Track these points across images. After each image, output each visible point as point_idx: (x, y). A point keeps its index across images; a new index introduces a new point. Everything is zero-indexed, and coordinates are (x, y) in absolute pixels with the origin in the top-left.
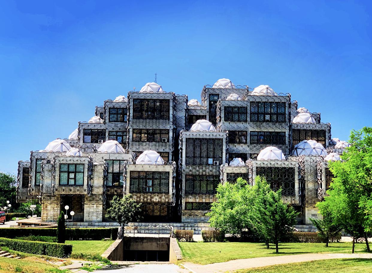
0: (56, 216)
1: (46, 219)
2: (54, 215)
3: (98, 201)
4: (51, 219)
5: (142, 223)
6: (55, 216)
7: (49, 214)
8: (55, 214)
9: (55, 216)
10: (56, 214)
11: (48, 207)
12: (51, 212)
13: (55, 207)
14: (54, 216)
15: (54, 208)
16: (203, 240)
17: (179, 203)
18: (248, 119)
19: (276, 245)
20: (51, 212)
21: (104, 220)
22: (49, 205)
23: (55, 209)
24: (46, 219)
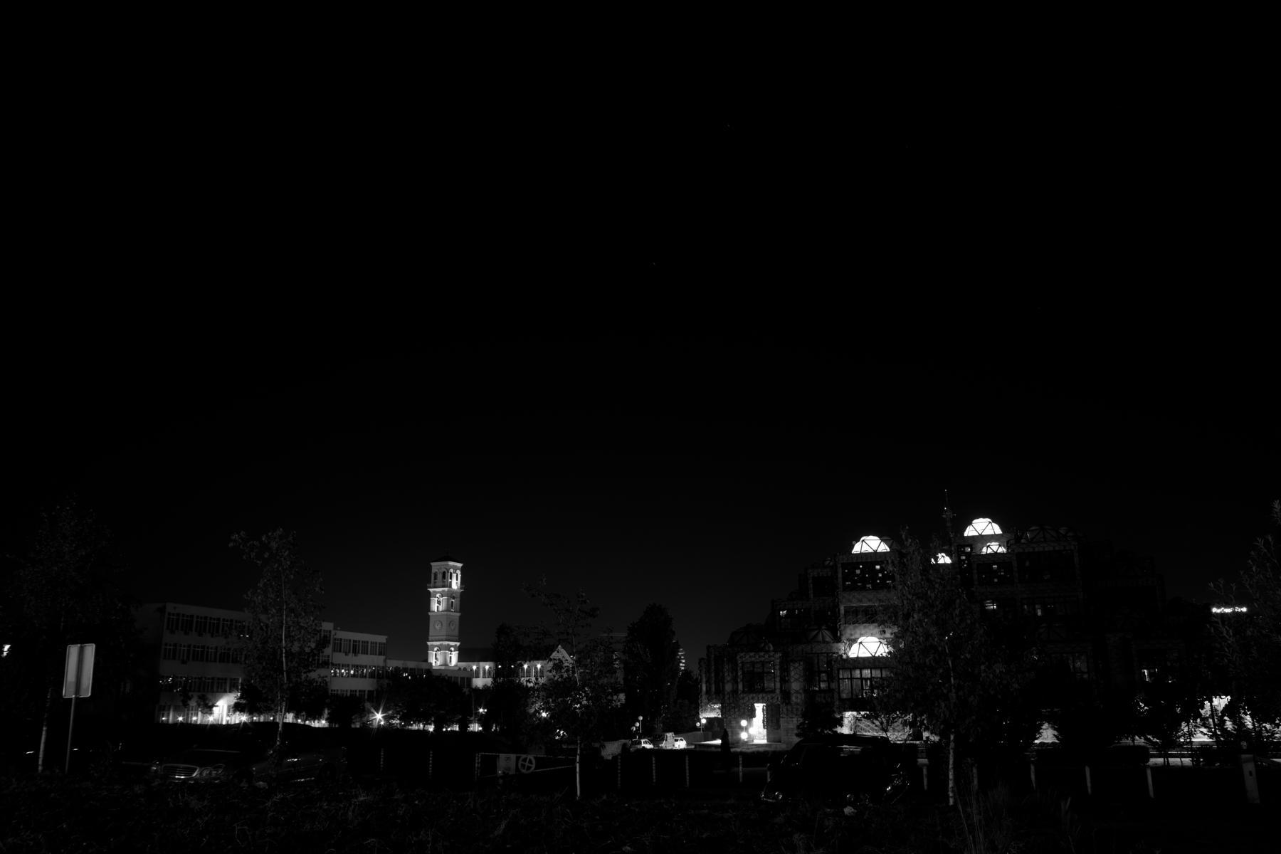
5: (482, 664)
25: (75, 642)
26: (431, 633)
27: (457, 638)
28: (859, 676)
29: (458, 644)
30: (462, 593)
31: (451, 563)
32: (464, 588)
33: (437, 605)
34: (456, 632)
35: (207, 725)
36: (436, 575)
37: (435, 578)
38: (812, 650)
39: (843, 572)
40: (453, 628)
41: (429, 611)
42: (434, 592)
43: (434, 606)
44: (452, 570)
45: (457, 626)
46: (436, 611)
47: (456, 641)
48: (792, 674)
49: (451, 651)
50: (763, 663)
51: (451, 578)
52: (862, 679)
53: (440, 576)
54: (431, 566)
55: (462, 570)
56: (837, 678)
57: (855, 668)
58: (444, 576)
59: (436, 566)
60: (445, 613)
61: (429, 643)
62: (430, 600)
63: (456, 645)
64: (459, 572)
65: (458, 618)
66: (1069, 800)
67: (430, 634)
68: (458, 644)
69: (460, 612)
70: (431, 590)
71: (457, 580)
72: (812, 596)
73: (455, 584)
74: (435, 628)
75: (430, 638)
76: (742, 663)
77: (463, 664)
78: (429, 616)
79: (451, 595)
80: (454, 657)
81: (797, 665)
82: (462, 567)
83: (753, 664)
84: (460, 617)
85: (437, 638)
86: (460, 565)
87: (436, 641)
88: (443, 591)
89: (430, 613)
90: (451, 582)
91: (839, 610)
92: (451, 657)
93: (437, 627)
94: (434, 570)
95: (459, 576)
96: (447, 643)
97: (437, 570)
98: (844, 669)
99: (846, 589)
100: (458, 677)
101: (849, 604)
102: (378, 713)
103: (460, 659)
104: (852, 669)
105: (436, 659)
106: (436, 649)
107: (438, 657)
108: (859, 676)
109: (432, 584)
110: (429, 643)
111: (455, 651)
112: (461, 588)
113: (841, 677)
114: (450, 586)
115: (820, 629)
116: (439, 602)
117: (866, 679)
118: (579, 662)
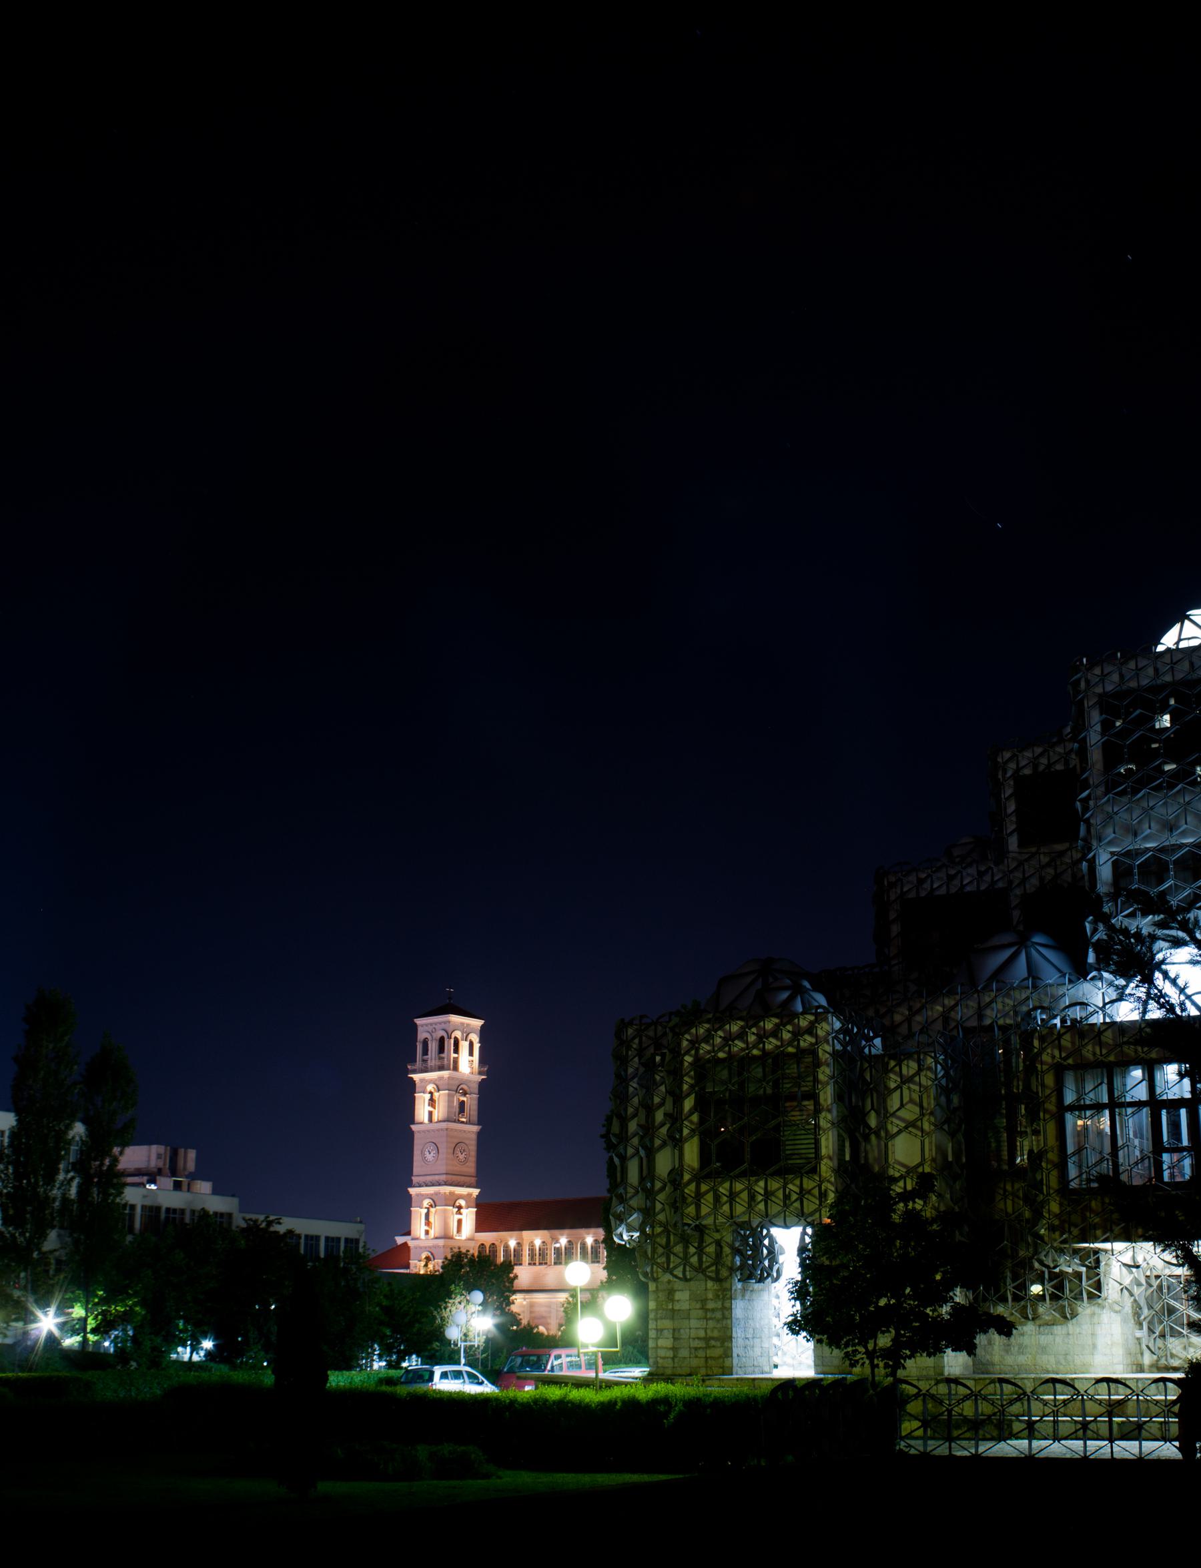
0: (718, 1344)
1: (673, 1359)
2: (707, 1339)
3: (677, 1204)
4: (695, 1362)
5: (527, 1235)
6: (713, 1343)
7: (684, 1334)
8: (710, 1334)
9: (713, 1343)
10: (716, 1334)
11: (678, 1296)
12: (694, 1323)
13: (710, 1296)
14: (708, 1347)
15: (706, 1299)
16: (913, 1359)
17: (1073, 708)
18: (302, 1241)
19: (186, 1149)
20: (694, 1323)
21: (974, 1373)
22: (678, 1284)
23: (711, 1305)
24: (673, 1359)
25: (871, 1339)
26: (417, 1169)
27: (473, 1180)
28: (1141, 1093)
29: (475, 1192)
30: (482, 1084)
31: (455, 1019)
32: (487, 1073)
33: (428, 1108)
34: (471, 1167)
35: (755, 1399)
36: (425, 1042)
37: (425, 1052)
38: (980, 1016)
39: (1107, 726)
40: (462, 1157)
41: (413, 1122)
42: (422, 1080)
43: (422, 1111)
44: (458, 1034)
45: (473, 1153)
46: (426, 1120)
47: (469, 1186)
48: (894, 1102)
49: (460, 1208)
50: (777, 1060)
51: (456, 1051)
52: (1155, 1103)
53: (433, 1047)
54: (415, 1026)
55: (484, 1033)
56: (1051, 1106)
57: (1127, 1064)
58: (441, 1049)
59: (427, 1026)
60: (444, 1125)
61: (412, 1191)
62: (414, 1098)
63: (470, 1195)
64: (475, 1038)
65: (474, 1137)
66: (1084, 776)
67: (416, 1170)
68: (475, 1192)
69: (478, 1124)
70: (416, 1077)
71: (471, 1054)
72: (1013, 843)
73: (468, 1064)
74: (425, 1159)
75: (415, 1179)
76: (698, 1063)
77: (488, 1237)
78: (412, 1133)
79: (458, 1088)
80: (469, 1217)
81: (909, 1068)
82: (482, 1027)
83: (743, 1063)
84: (479, 1134)
85: (429, 1178)
86: (478, 1023)
87: (462, 1186)
88: (441, 1078)
89: (413, 1127)
90: (456, 1061)
91: (1092, 864)
92: (460, 1222)
93: (430, 1157)
94: (421, 1035)
95: (477, 1046)
96: (447, 1189)
97: (427, 1035)
98: (1082, 1068)
99: (1111, 784)
100: (317, 1238)
101: (1128, 844)
102: (46, 1314)
103: (481, 1226)
104: (1113, 1068)
105: (428, 1223)
106: (426, 1203)
107: (432, 1219)
108: (1141, 1093)
109: (419, 1064)
110: (412, 1191)
111: (468, 1207)
112: (480, 1073)
113: (1070, 1097)
114: (456, 1068)
115: (1023, 942)
116: (432, 1101)
117: (1174, 1105)
118: (1043, 1284)
